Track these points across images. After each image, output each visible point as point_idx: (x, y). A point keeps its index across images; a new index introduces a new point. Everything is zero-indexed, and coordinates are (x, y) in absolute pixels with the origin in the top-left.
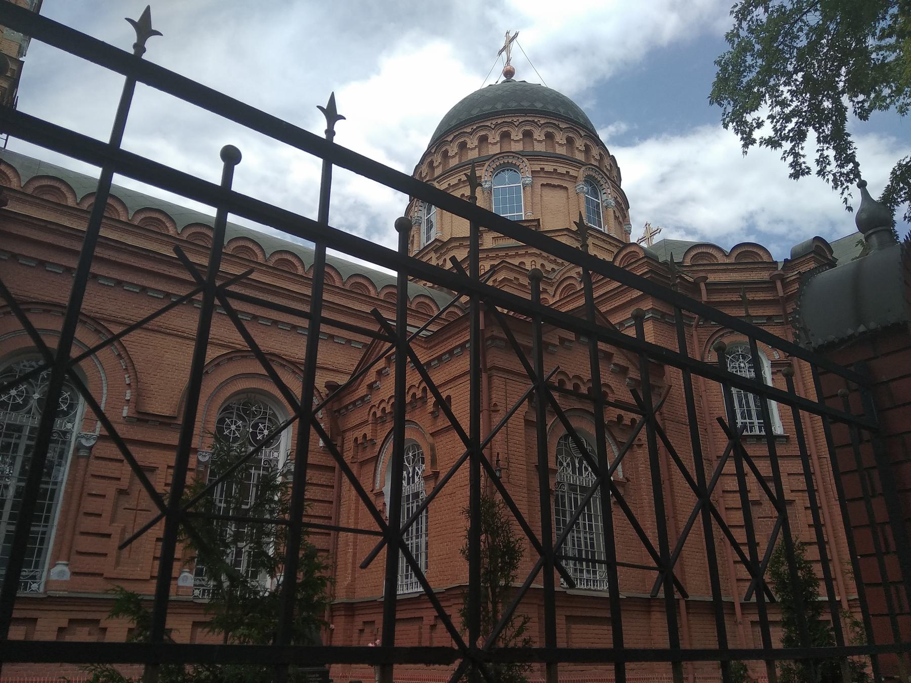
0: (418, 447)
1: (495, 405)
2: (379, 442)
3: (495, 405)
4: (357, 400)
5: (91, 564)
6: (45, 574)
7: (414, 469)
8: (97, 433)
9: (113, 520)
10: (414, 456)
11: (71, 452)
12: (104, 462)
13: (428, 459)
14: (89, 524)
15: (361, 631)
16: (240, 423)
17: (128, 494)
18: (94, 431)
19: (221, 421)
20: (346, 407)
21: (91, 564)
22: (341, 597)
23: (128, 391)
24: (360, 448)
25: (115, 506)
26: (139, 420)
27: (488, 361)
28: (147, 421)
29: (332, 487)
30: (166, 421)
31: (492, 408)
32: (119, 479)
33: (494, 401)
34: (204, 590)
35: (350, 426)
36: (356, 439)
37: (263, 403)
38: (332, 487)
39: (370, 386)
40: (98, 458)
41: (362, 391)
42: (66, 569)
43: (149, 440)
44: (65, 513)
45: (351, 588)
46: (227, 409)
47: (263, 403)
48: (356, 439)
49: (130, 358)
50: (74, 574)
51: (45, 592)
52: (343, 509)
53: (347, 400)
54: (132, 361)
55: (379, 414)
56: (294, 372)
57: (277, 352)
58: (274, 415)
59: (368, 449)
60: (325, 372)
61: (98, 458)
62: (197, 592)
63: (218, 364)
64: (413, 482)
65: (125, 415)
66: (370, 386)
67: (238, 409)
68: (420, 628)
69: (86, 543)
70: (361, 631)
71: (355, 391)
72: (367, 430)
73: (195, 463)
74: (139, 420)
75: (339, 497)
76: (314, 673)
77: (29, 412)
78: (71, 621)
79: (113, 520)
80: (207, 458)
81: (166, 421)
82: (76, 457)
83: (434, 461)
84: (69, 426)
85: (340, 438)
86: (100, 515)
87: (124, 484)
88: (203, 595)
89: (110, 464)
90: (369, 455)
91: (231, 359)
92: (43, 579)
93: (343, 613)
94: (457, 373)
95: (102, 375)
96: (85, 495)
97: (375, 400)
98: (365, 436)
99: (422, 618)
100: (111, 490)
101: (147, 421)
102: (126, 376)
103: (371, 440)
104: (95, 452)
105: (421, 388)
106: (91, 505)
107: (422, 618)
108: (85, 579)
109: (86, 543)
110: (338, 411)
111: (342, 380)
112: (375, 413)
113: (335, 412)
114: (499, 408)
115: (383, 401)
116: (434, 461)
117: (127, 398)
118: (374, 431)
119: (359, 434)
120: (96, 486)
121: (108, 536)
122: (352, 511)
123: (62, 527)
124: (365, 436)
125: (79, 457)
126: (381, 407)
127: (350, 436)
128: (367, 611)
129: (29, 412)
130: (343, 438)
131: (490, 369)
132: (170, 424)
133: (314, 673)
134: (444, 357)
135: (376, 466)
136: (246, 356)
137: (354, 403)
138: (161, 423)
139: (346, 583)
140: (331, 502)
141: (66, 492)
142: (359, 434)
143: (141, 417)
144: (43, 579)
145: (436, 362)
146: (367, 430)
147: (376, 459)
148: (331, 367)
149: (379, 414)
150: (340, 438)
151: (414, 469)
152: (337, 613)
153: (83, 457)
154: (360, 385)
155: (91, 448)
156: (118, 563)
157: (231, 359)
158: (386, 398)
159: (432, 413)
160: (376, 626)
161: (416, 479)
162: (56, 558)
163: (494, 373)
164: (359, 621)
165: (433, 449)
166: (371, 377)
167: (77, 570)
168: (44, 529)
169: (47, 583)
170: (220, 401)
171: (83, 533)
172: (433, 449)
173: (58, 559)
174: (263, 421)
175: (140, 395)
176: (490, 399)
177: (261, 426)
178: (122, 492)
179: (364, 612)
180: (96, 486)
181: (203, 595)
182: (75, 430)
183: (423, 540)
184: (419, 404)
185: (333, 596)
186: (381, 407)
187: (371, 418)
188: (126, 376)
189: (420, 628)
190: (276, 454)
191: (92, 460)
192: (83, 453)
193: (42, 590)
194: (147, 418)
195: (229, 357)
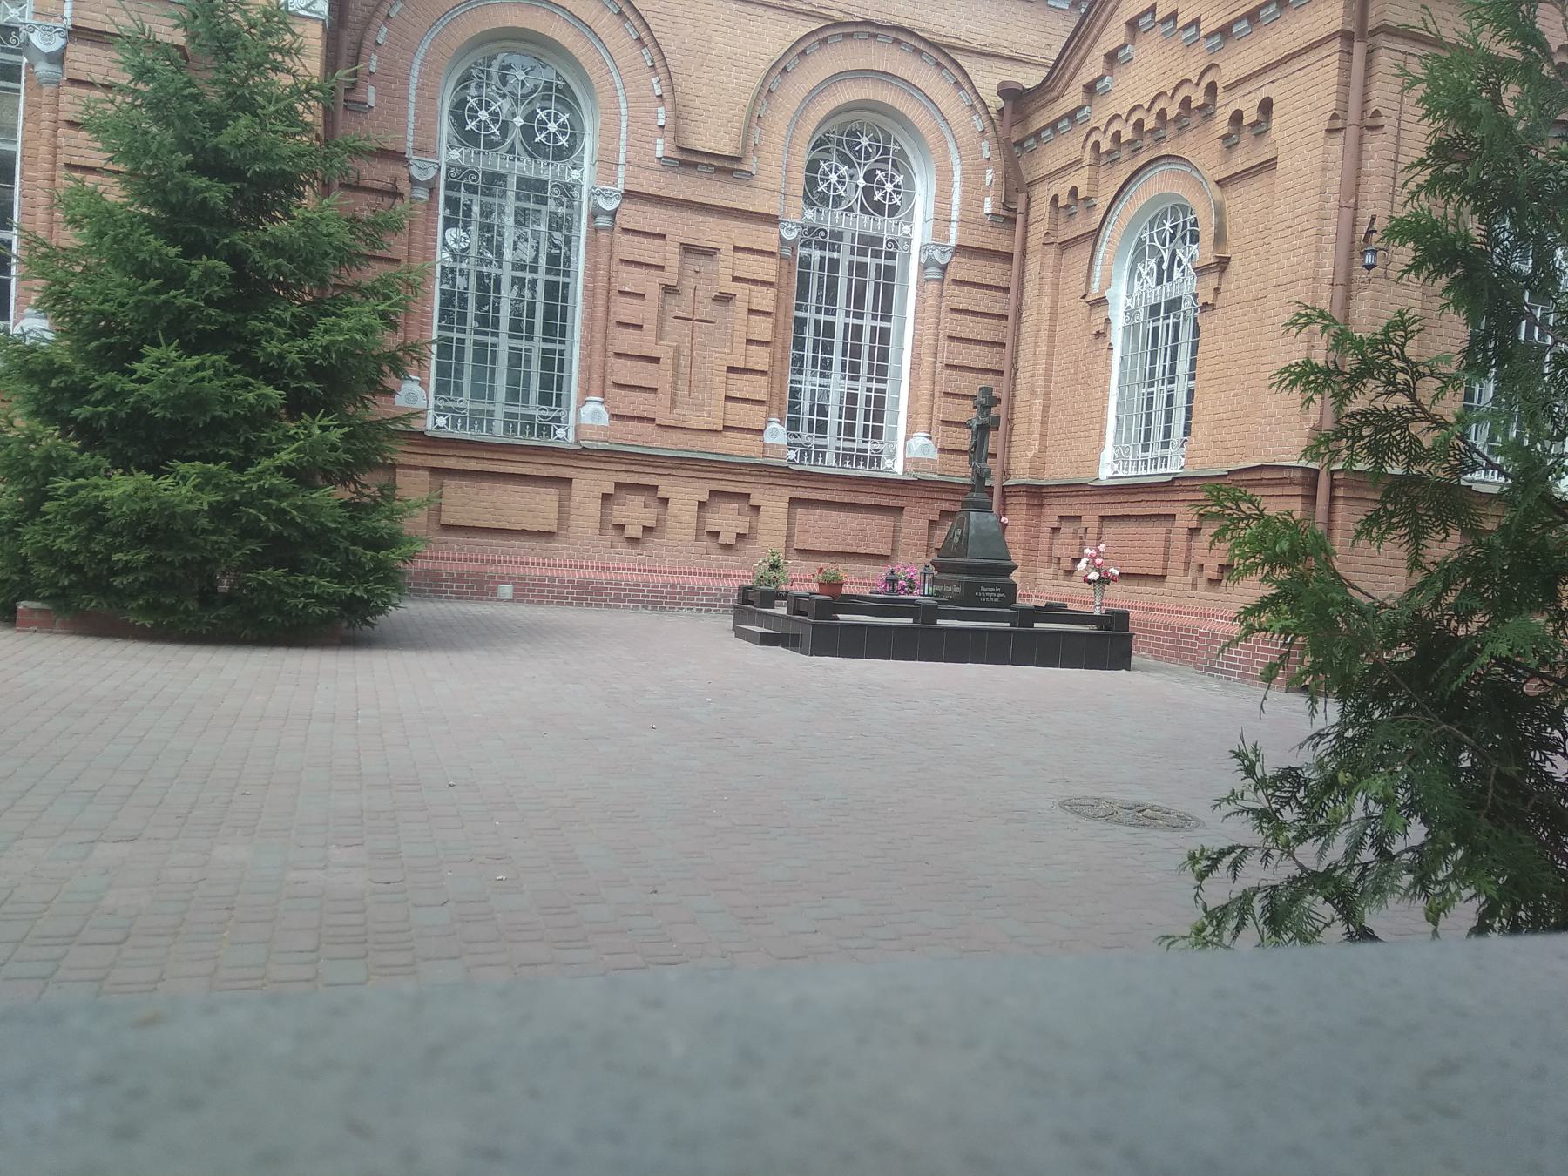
0: (1186, 209)
1: (1377, 114)
2: (1102, 203)
3: (1377, 114)
4: (1061, 119)
5: (637, 403)
6: (572, 415)
7: (1173, 254)
8: (953, 243)
9: (660, 336)
10: (1174, 228)
11: (584, 220)
12: (636, 239)
13: (1207, 232)
14: (625, 341)
15: (1055, 530)
16: (844, 169)
17: (677, 293)
18: (615, 183)
19: (812, 166)
20: (1037, 135)
21: (637, 403)
22: (1021, 474)
23: (660, 110)
24: (1062, 215)
25: (662, 311)
26: (682, 163)
27: (1372, 13)
28: (695, 165)
29: (1007, 290)
30: (726, 164)
31: (1369, 122)
32: (662, 268)
33: (1374, 105)
34: (802, 452)
35: (1043, 172)
36: (1055, 199)
37: (882, 130)
38: (1007, 290)
39: (1090, 89)
40: (626, 231)
41: (1073, 97)
42: (601, 408)
43: (701, 200)
44: (589, 321)
45: (1038, 463)
46: (820, 144)
47: (882, 130)
48: (1055, 199)
49: (657, 45)
50: (613, 416)
51: (577, 442)
52: (1027, 329)
53: (1040, 120)
54: (661, 52)
55: (1105, 145)
56: (938, 64)
57: (906, 23)
58: (902, 153)
59: (1077, 218)
60: (997, 63)
61: (626, 231)
62: (792, 455)
63: (804, 52)
64: (1170, 278)
65: (659, 154)
66: (1090, 89)
67: (840, 143)
68: (1168, 532)
69: (626, 372)
70: (1055, 530)
71: (1056, 99)
72: (1080, 179)
73: (777, 243)
74: (682, 163)
75: (1019, 309)
76: (993, 585)
77: (511, 150)
78: (713, 494)
79: (660, 336)
80: (794, 235)
81: (726, 164)
82: (594, 230)
83: (1220, 237)
84: (575, 174)
85: (1022, 198)
86: (640, 327)
87: (670, 277)
88: (802, 459)
89: (646, 240)
90: (1079, 227)
91: (825, 40)
92: (572, 423)
93: (1025, 500)
94: (1294, 47)
95: (617, 79)
96: (614, 292)
97: (1098, 115)
98: (1074, 192)
99: (570, 481)
100: (650, 284)
101: (695, 165)
102: (655, 80)
103: (1087, 199)
104: (622, 221)
105: (1203, 84)
106: (626, 310)
107: (570, 481)
108: (632, 425)
109: (626, 372)
110: (1020, 143)
111: (1029, 78)
112: (1096, 145)
113: (1015, 144)
114: (1381, 121)
115: (1117, 116)
116: (1220, 237)
117: (661, 122)
118: (1094, 180)
119: (1061, 188)
120: (630, 279)
121: (656, 360)
122: (1044, 335)
123: (588, 343)
124: (1074, 192)
125: (596, 230)
126: (1112, 130)
127: (1043, 194)
128: (1067, 500)
129: (511, 150)
130: (1029, 198)
131: (1374, 33)
132: (731, 172)
133: (993, 585)
134: (1263, 13)
135: (1094, 250)
136: (851, 35)
137: (1053, 126)
138: (718, 170)
139: (1030, 454)
140: (1005, 318)
141: (585, 286)
142: (1061, 188)
143: (685, 157)
144: (572, 423)
145: (1245, 24)
146: (1080, 179)
147: (1095, 235)
148: (1007, 53)
149: (1105, 145)
150: (1022, 198)
151: (1173, 254)
152: (1014, 500)
153: (605, 229)
154: (1067, 86)
155: (613, 214)
156: (674, 404)
157: (825, 40)
158: (1124, 112)
159: (1225, 138)
160: (1084, 524)
161: (1177, 273)
162: (586, 391)
163: (1381, 40)
164: (1051, 517)
165: (1220, 212)
166: (1093, 67)
167: (616, 412)
168: (562, 347)
169: (577, 428)
170: (809, 127)
171: (618, 355)
172: (1220, 212)
173: (588, 393)
174: (882, 165)
175: (679, 116)
176: (1365, 101)
177: (880, 175)
178: (669, 290)
179: (1062, 501)
180: (630, 279)
181: (802, 459)
182: (585, 181)
183: (1181, 387)
184: (1195, 119)
185: (1006, 473)
186: (1112, 130)
187: (1087, 155)
188: (655, 80)
189: (1168, 532)
190: (906, 229)
191: (617, 235)
192: (603, 222)
193: (571, 438)
194: (695, 159)
195: (821, 36)
